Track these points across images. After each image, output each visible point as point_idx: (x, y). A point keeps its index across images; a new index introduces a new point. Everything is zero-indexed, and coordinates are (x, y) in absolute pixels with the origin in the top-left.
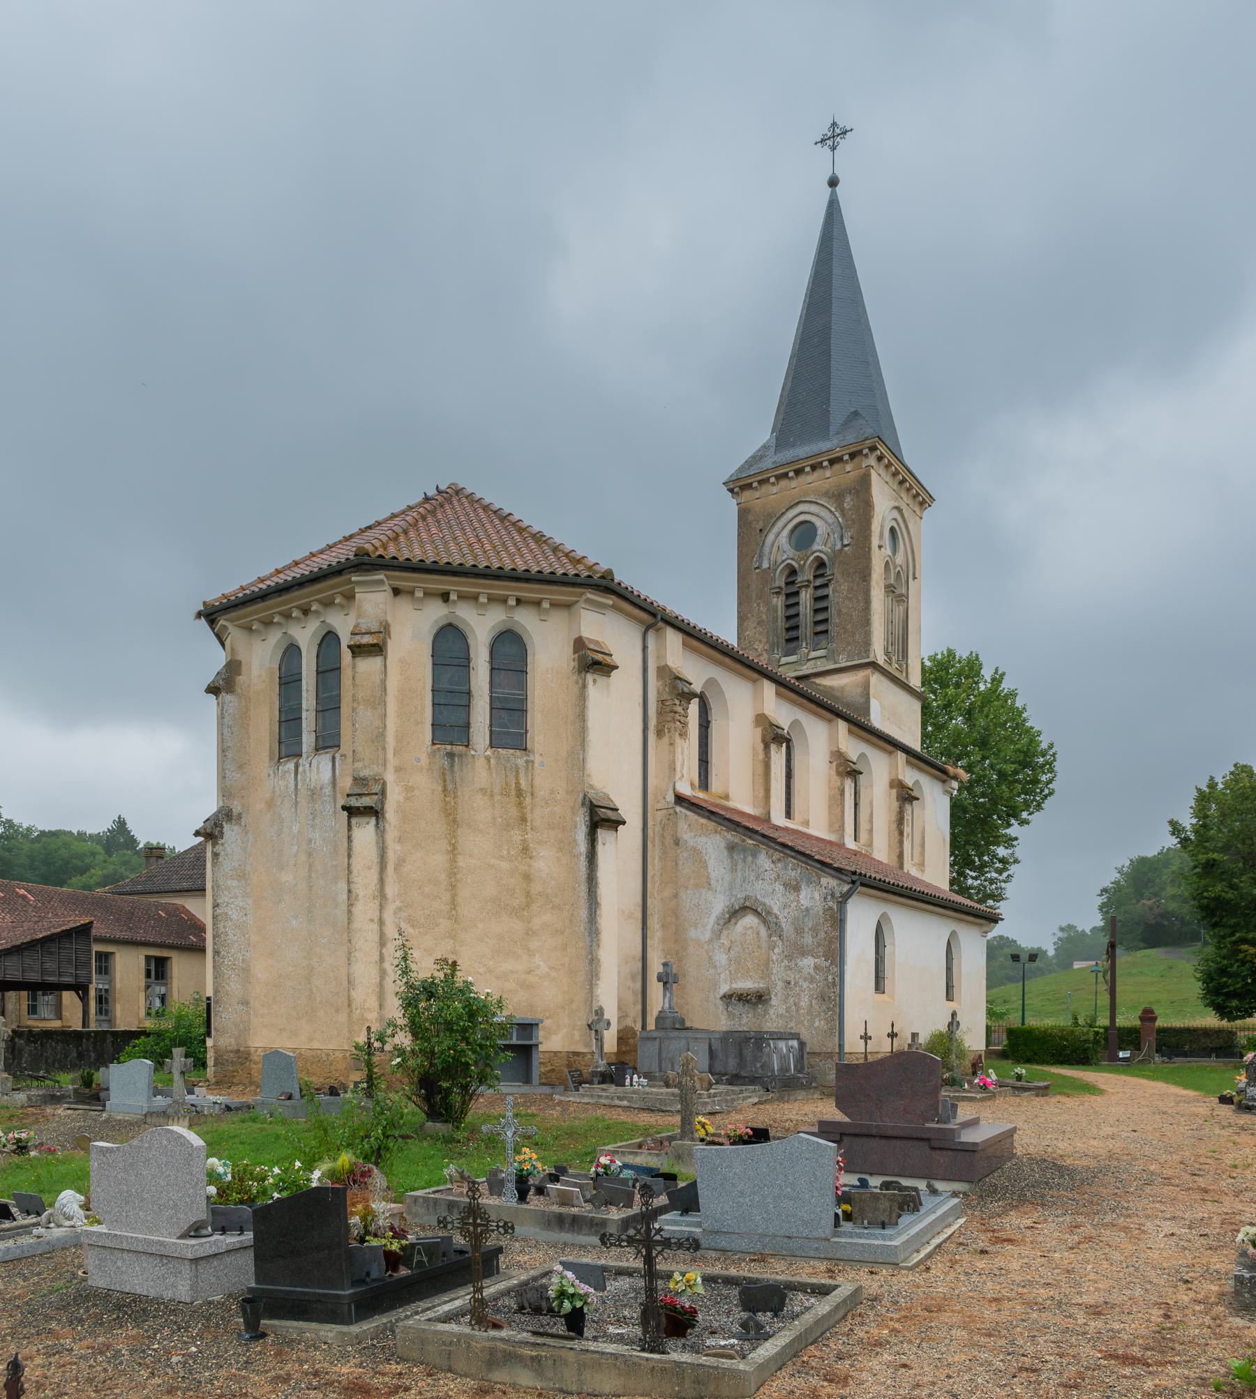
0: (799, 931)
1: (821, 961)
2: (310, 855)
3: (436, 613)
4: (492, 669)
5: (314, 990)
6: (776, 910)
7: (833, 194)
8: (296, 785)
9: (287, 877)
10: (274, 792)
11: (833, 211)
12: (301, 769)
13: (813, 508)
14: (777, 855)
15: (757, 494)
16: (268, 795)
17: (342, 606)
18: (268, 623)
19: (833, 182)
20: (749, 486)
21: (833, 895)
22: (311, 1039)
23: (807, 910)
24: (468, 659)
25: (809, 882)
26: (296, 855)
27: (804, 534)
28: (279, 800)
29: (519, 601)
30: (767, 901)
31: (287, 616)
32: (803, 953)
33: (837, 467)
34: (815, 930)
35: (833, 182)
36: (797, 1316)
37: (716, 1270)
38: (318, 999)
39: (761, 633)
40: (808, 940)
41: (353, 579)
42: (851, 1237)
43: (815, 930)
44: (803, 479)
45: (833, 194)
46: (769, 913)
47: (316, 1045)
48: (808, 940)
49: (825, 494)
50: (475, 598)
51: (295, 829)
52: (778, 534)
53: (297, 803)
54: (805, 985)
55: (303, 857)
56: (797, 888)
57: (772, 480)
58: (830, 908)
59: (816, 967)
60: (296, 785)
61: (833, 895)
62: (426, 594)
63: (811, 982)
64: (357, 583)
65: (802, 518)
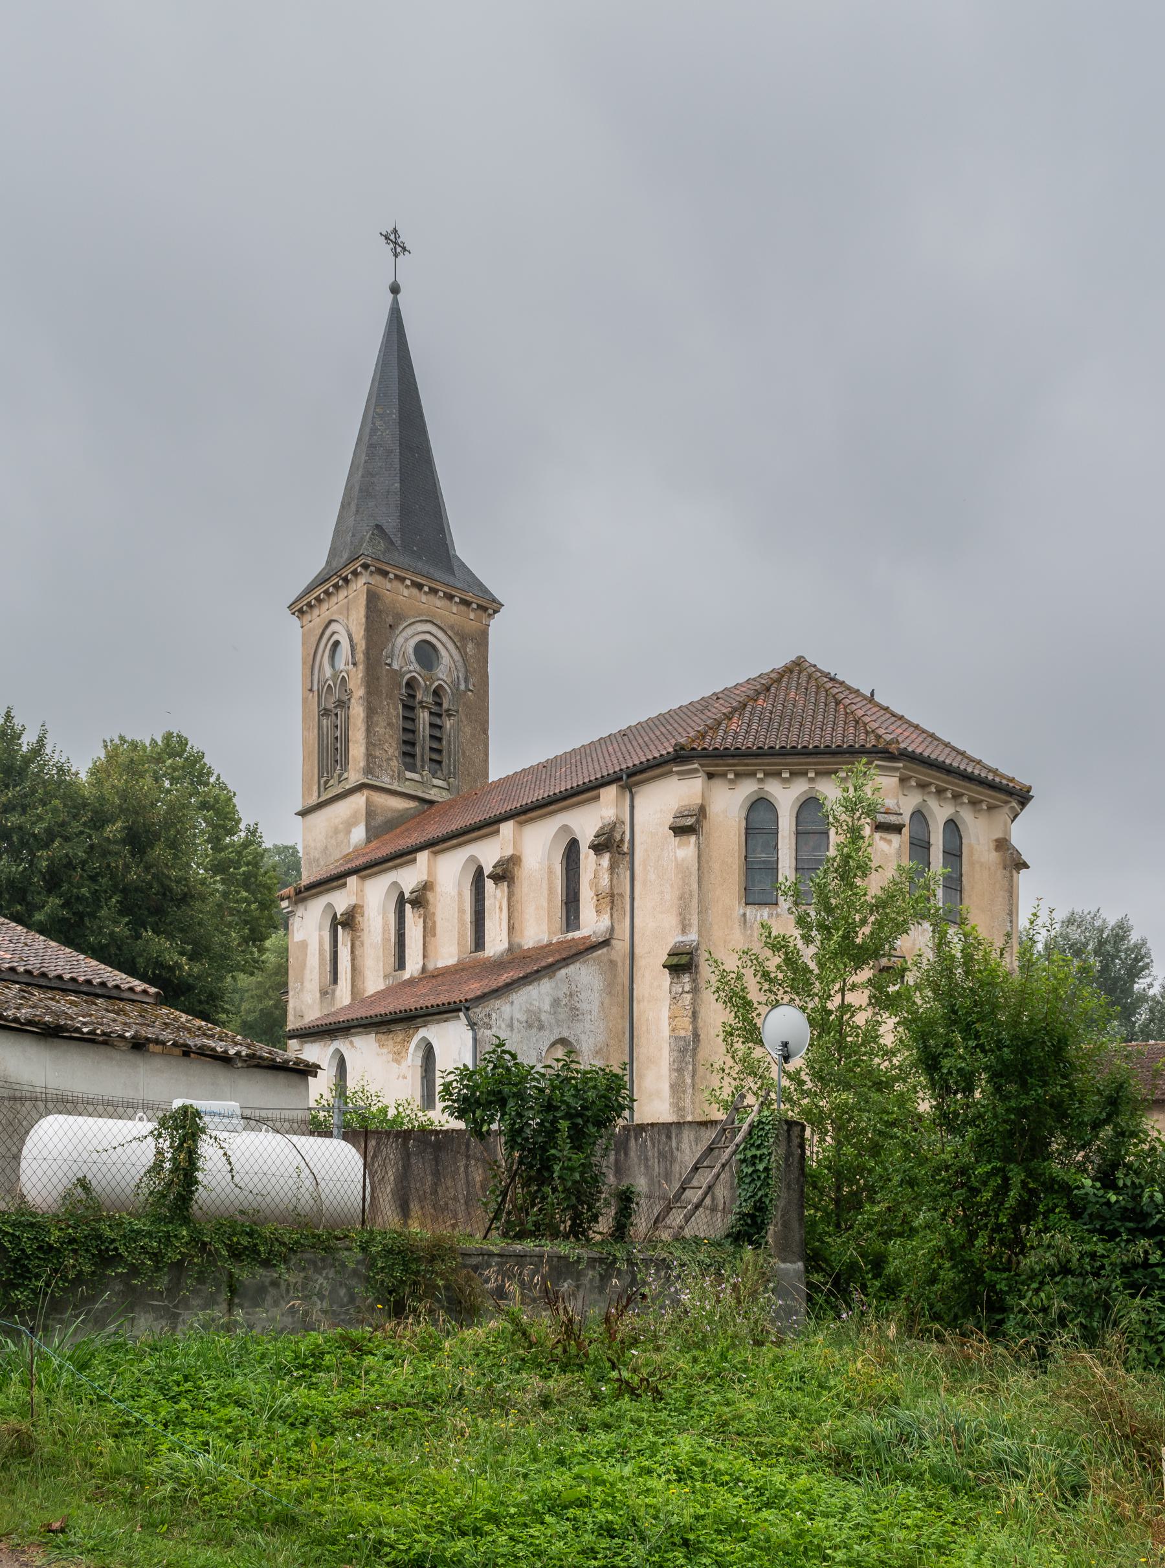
3: (747, 789)
4: (798, 833)
7: (395, 302)
13: (440, 634)
17: (731, 781)
18: (922, 786)
19: (395, 289)
24: (747, 834)
27: (426, 653)
29: (737, 775)
31: (940, 792)
33: (463, 608)
35: (395, 289)
36: (696, 1036)
39: (391, 736)
42: (927, 846)
44: (432, 598)
45: (395, 302)
49: (452, 628)
50: (778, 774)
52: (407, 640)
57: (426, 589)
62: (791, 774)
65: (428, 637)
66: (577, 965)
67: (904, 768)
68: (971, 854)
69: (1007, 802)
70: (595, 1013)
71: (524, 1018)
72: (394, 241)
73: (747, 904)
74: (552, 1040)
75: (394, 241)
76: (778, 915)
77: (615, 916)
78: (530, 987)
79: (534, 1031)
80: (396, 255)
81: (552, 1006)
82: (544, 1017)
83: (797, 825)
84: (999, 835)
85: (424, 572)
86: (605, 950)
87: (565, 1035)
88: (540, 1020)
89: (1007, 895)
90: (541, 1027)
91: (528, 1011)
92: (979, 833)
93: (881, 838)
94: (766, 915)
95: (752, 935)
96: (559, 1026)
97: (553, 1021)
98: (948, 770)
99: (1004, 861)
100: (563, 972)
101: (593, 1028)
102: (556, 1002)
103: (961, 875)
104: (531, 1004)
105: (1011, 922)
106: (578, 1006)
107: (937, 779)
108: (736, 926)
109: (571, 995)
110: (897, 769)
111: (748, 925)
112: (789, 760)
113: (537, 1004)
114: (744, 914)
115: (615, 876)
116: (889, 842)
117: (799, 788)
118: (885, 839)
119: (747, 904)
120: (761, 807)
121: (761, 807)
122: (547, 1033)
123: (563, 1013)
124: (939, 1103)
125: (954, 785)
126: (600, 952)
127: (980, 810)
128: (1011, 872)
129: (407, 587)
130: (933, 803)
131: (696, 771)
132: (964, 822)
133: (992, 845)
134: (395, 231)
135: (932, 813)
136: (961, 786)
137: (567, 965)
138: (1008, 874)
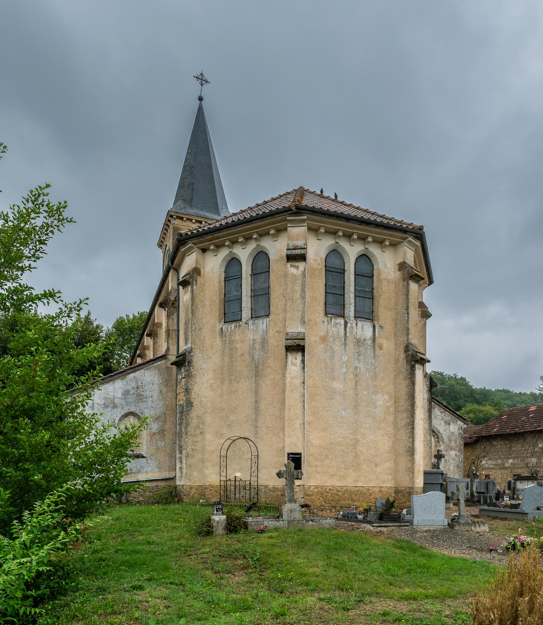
0: (450, 441)
1: (457, 453)
2: (356, 376)
5: (359, 452)
6: (441, 432)
7: (200, 104)
8: (345, 334)
9: (338, 385)
10: (327, 333)
11: (200, 110)
12: (349, 325)
14: (442, 410)
15: (184, 224)
16: (322, 334)
18: (334, 233)
19: (201, 99)
20: (182, 219)
21: (461, 428)
22: (356, 481)
23: (453, 433)
25: (453, 422)
26: (345, 374)
28: (331, 339)
30: (438, 427)
32: (451, 449)
34: (455, 440)
35: (201, 99)
37: (322, 596)
38: (362, 458)
40: (453, 444)
41: (288, 218)
43: (455, 440)
45: (200, 104)
46: (439, 432)
47: (360, 484)
48: (453, 444)
51: (345, 358)
53: (345, 344)
54: (452, 461)
55: (351, 376)
56: (449, 424)
57: (194, 221)
58: (461, 433)
59: (456, 455)
60: (345, 334)
61: (461, 428)
63: (454, 460)
64: (290, 221)
66: (143, 371)
67: (308, 219)
68: (379, 275)
69: (405, 239)
70: (155, 397)
71: (103, 402)
72: (202, 79)
73: (225, 322)
74: (123, 413)
75: (202, 79)
76: (240, 326)
77: (170, 342)
78: (108, 385)
79: (109, 409)
80: (202, 85)
81: (123, 394)
82: (117, 401)
83: (252, 270)
84: (400, 260)
85: (202, 215)
86: (163, 361)
87: (133, 409)
88: (114, 403)
89: (405, 297)
90: (115, 407)
91: (105, 398)
92: (387, 263)
93: (291, 266)
94: (233, 327)
95: (225, 340)
96: (128, 405)
97: (124, 403)
98: (348, 219)
99: (403, 275)
100: (132, 375)
101: (153, 405)
102: (126, 393)
103: (373, 289)
104: (108, 394)
105: (408, 313)
106: (143, 393)
107: (342, 227)
108: (218, 336)
109: (138, 388)
110: (304, 221)
111: (224, 334)
112: (239, 229)
113: (112, 394)
114: (222, 328)
115: (171, 320)
116: (297, 267)
117: (252, 246)
118: (294, 266)
119: (225, 322)
120: (233, 263)
121: (233, 263)
122: (119, 410)
123: (131, 398)
124: (529, 413)
125: (357, 230)
126: (159, 363)
127: (385, 246)
128: (408, 282)
129: (194, 223)
130: (344, 244)
131: (191, 248)
132: (373, 255)
133: (397, 268)
134: (202, 74)
135: (345, 251)
136: (364, 230)
137: (135, 371)
138: (406, 284)
